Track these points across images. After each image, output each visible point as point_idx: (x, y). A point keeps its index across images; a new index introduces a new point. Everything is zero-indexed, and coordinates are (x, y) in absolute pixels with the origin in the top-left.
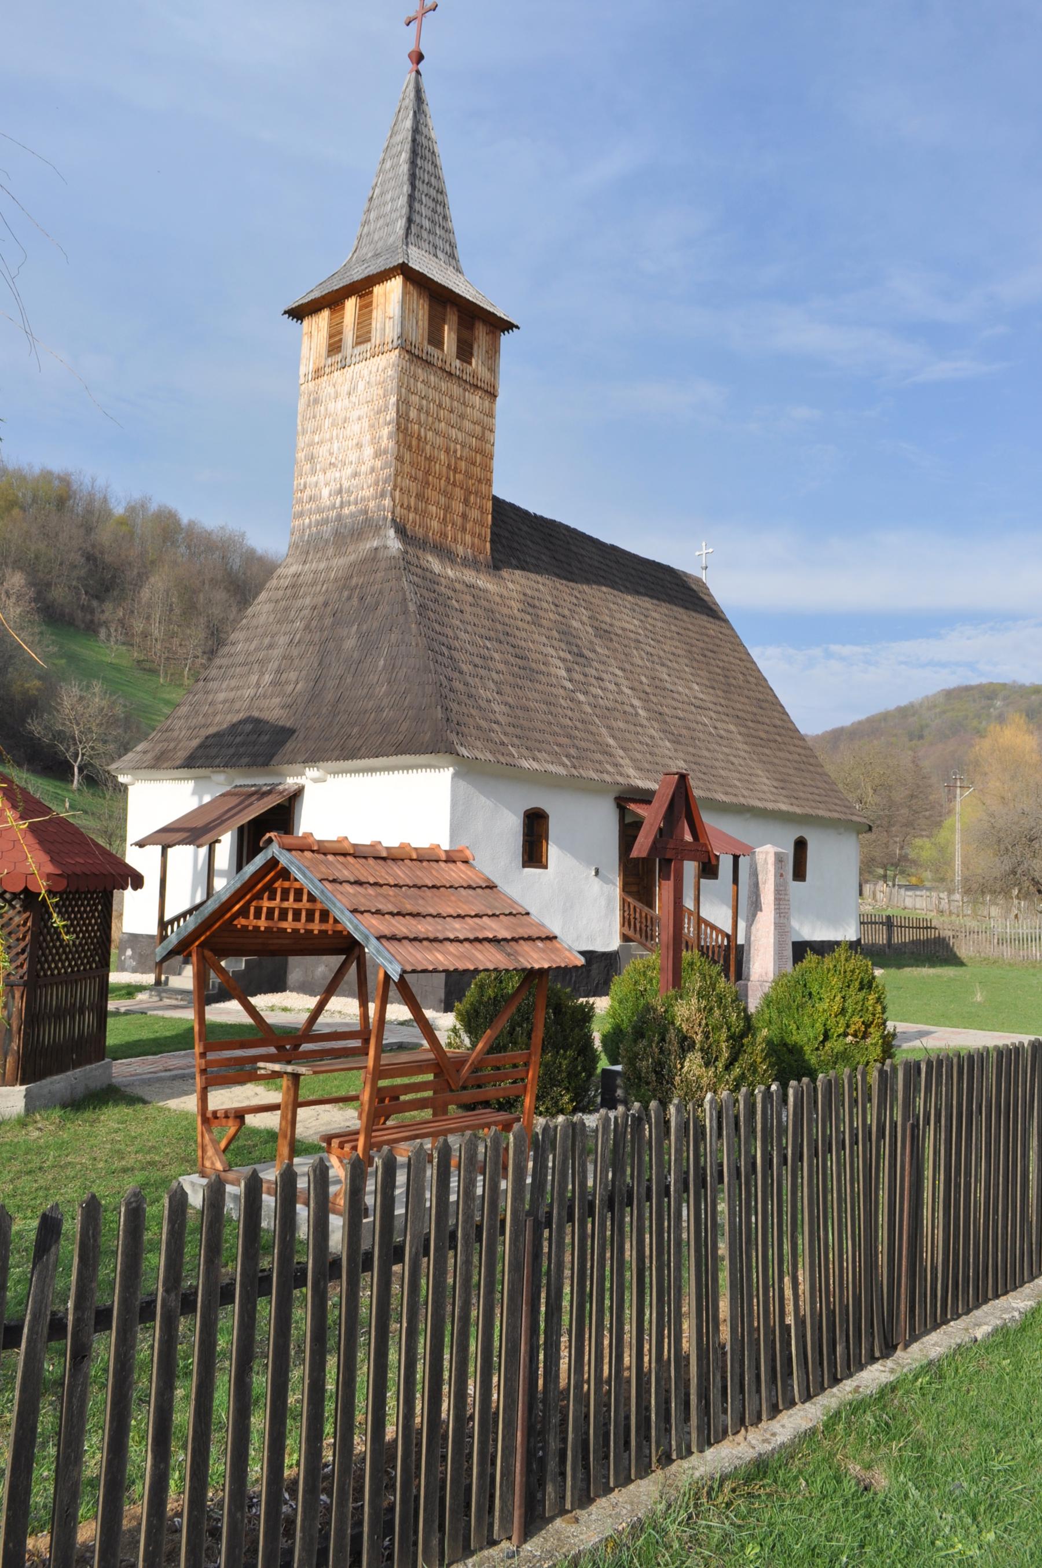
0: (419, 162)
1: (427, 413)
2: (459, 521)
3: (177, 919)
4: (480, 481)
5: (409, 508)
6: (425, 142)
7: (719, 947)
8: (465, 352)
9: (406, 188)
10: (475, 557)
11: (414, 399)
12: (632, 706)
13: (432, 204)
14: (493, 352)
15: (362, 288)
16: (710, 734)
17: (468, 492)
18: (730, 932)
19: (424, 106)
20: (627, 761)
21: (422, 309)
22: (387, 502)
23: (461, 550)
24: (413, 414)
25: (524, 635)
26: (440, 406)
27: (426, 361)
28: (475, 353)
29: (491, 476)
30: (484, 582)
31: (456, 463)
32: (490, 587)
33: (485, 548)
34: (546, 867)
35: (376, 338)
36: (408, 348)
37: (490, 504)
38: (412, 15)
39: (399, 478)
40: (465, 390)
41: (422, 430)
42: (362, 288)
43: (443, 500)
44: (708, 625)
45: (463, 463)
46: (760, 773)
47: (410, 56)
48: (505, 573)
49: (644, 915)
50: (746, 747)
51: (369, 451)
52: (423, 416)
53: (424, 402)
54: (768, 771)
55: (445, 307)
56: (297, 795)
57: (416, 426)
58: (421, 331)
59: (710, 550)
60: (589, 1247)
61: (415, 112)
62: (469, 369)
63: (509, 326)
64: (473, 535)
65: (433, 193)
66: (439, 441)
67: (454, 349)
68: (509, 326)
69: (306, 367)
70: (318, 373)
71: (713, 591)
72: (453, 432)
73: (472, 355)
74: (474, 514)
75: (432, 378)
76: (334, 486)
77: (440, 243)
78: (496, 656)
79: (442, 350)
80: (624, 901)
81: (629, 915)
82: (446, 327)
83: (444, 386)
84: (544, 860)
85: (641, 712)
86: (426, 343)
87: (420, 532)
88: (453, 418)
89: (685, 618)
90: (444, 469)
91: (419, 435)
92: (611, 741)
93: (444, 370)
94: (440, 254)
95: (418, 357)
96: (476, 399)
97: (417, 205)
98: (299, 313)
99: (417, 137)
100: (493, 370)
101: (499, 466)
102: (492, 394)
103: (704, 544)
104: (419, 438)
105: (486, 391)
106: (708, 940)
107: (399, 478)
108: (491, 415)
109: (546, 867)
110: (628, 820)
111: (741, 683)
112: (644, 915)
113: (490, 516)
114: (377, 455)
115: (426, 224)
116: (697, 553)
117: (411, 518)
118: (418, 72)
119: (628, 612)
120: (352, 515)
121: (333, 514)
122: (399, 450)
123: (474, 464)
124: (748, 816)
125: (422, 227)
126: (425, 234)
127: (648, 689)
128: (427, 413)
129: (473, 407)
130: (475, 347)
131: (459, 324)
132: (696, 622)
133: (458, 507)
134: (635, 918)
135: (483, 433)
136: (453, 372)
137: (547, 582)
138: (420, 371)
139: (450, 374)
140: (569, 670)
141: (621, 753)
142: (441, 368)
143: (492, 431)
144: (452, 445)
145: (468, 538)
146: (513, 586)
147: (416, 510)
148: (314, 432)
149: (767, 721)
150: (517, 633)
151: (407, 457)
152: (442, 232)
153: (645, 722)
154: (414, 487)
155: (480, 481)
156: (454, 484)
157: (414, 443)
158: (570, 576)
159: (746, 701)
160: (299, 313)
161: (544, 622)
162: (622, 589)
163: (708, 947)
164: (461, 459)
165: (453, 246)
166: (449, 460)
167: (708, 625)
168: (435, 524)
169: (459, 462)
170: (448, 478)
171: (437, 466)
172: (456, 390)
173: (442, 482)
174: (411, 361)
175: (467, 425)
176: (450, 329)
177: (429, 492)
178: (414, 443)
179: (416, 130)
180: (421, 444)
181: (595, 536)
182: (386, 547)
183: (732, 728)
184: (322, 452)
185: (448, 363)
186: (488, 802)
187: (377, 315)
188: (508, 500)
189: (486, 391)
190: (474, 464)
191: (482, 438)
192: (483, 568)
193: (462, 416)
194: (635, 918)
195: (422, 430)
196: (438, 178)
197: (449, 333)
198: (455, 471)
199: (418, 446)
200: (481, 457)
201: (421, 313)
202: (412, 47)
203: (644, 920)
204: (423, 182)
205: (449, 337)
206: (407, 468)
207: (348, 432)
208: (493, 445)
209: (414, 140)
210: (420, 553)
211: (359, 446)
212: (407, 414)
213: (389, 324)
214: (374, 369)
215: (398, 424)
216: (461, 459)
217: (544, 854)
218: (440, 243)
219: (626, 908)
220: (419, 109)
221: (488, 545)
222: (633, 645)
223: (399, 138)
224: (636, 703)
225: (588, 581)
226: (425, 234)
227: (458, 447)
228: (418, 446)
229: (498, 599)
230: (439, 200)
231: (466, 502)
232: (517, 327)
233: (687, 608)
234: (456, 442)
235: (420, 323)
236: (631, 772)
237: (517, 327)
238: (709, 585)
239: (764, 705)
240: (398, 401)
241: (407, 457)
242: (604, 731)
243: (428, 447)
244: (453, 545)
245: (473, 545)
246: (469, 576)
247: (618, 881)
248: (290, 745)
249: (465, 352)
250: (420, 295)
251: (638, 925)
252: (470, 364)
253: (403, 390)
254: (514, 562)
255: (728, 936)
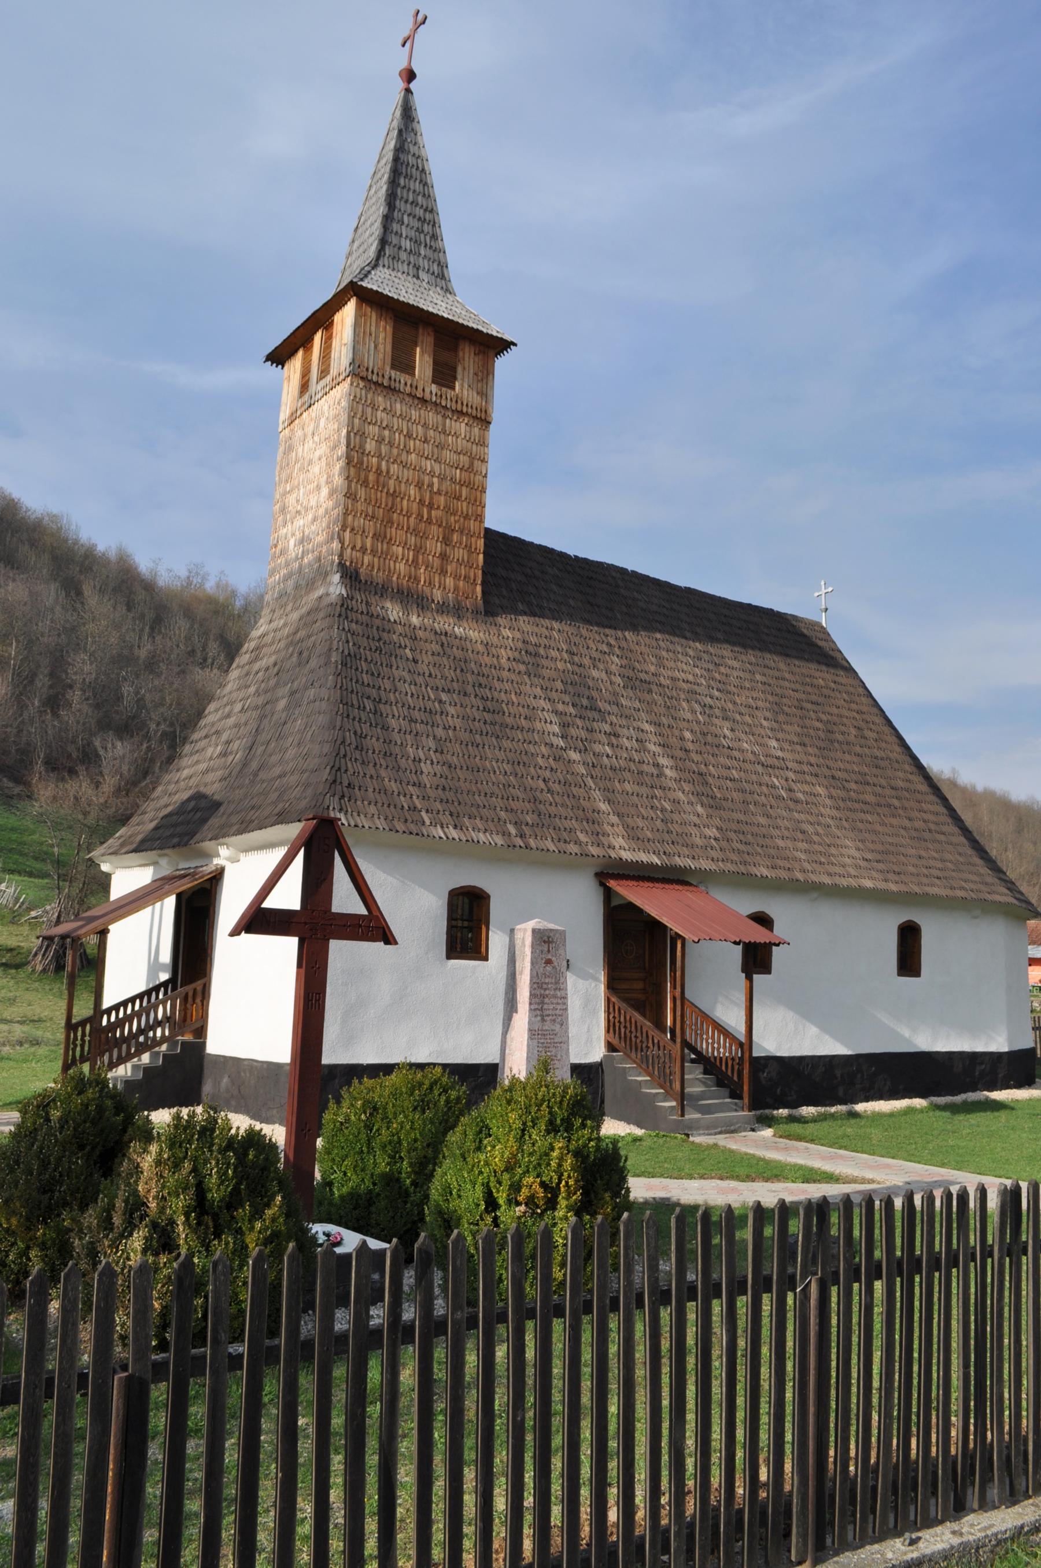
0: (402, 182)
1: (391, 444)
2: (437, 562)
3: (116, 1007)
4: (467, 517)
5: (363, 550)
6: (412, 160)
7: (733, 1059)
8: (444, 375)
9: (382, 209)
10: (458, 602)
11: (373, 430)
12: (657, 765)
13: (416, 224)
14: (485, 374)
15: (322, 319)
16: (779, 797)
17: (449, 530)
18: (743, 1039)
19: (415, 124)
20: (620, 830)
21: (383, 333)
22: (336, 545)
23: (438, 595)
24: (370, 446)
25: (507, 686)
26: (409, 435)
27: (389, 387)
28: (459, 376)
29: (483, 512)
30: (470, 631)
31: (431, 498)
32: (473, 634)
33: (474, 591)
34: (486, 958)
35: (334, 371)
36: (364, 374)
37: (481, 543)
38: (406, 35)
39: (350, 518)
40: (444, 417)
41: (384, 463)
42: (322, 319)
43: (412, 540)
44: (812, 672)
45: (442, 498)
46: (848, 843)
47: (400, 74)
48: (501, 620)
49: (628, 1018)
50: (834, 813)
51: (325, 491)
52: (384, 449)
53: (386, 433)
54: (862, 841)
55: (417, 329)
56: (217, 876)
57: (375, 460)
58: (381, 356)
59: (830, 589)
60: (989, 1306)
61: (400, 132)
62: (450, 393)
63: (502, 345)
64: (456, 577)
65: (419, 212)
66: (406, 474)
67: (429, 373)
68: (502, 345)
69: (284, 414)
70: (293, 418)
71: (834, 636)
72: (428, 465)
73: (455, 378)
74: (460, 553)
75: (398, 406)
76: (298, 535)
77: (423, 263)
78: (452, 710)
79: (414, 375)
80: (608, 1000)
81: (614, 1017)
82: (418, 350)
83: (414, 414)
84: (483, 949)
85: (668, 772)
86: (388, 368)
87: (379, 577)
88: (428, 449)
89: (782, 666)
90: (415, 506)
91: (379, 468)
92: (604, 807)
93: (415, 397)
94: (423, 275)
95: (376, 383)
96: (461, 427)
97: (395, 226)
98: (279, 357)
99: (401, 156)
100: (485, 394)
101: (491, 499)
102: (484, 421)
103: (823, 583)
104: (379, 472)
105: (475, 418)
106: (722, 1050)
107: (350, 518)
108: (483, 443)
109: (486, 958)
110: (615, 902)
111: (852, 738)
112: (628, 1018)
113: (481, 556)
114: (331, 494)
115: (407, 244)
116: (816, 594)
117: (366, 561)
118: (408, 91)
119: (680, 662)
120: (310, 564)
121: (296, 565)
122: (349, 487)
123: (458, 498)
124: (815, 895)
125: (400, 248)
126: (403, 256)
127: (690, 746)
128: (391, 444)
129: (456, 435)
130: (459, 369)
131: (435, 345)
132: (795, 669)
133: (434, 546)
134: (619, 1022)
135: (471, 464)
136: (427, 397)
137: (566, 628)
138: (380, 399)
139: (423, 401)
140: (564, 725)
141: (614, 819)
142: (410, 395)
143: (483, 461)
144: (426, 479)
145: (449, 582)
146: (511, 631)
147: (373, 552)
148: (287, 481)
149: (883, 782)
150: (496, 684)
151: (362, 493)
152: (429, 253)
153: (673, 785)
154: (370, 526)
155: (467, 517)
156: (429, 522)
157: (372, 477)
158: (608, 622)
159: (855, 759)
160: (279, 357)
161: (546, 673)
162: (688, 635)
163: (721, 1058)
164: (439, 493)
165: (443, 266)
166: (421, 496)
167: (818, 674)
168: (401, 567)
169: (436, 497)
170: (420, 515)
171: (405, 502)
172: (432, 417)
173: (412, 520)
174: (368, 389)
175: (448, 455)
176: (422, 353)
177: (392, 532)
178: (372, 477)
179: (400, 149)
180: (382, 479)
181: (663, 577)
182: (328, 594)
183: (820, 790)
184: (291, 500)
185: (420, 389)
186: (390, 879)
187: (336, 343)
188: (537, 542)
189: (475, 418)
190: (458, 498)
191: (470, 469)
192: (469, 614)
193: (441, 446)
194: (619, 1022)
195: (384, 463)
196: (428, 196)
197: (422, 355)
198: (431, 507)
199: (378, 481)
200: (472, 490)
201: (382, 335)
202: (404, 65)
203: (628, 1025)
204: (406, 202)
205: (423, 362)
206: (360, 506)
207: (310, 475)
208: (485, 476)
209: (396, 160)
210: (373, 600)
211: (318, 488)
212: (362, 447)
213: (344, 350)
214: (332, 403)
215: (347, 457)
216: (439, 493)
217: (483, 942)
218: (423, 263)
219: (611, 1009)
220: (407, 128)
221: (479, 589)
222: (683, 696)
223: (383, 161)
224: (664, 761)
225: (634, 628)
226: (403, 256)
227: (435, 480)
228: (378, 481)
229: (481, 648)
230: (428, 221)
231: (446, 541)
232: (515, 345)
233: (787, 655)
234: (432, 474)
235: (381, 347)
236: (619, 842)
237: (515, 345)
238: (829, 630)
239: (882, 763)
240: (348, 433)
241: (362, 493)
242: (597, 794)
243: (391, 482)
244: (427, 590)
245: (456, 588)
246: (444, 623)
247: (602, 977)
248: (214, 821)
249: (444, 375)
250: (380, 317)
251: (623, 1030)
252: (453, 388)
253: (356, 421)
254: (520, 606)
255: (741, 1045)
